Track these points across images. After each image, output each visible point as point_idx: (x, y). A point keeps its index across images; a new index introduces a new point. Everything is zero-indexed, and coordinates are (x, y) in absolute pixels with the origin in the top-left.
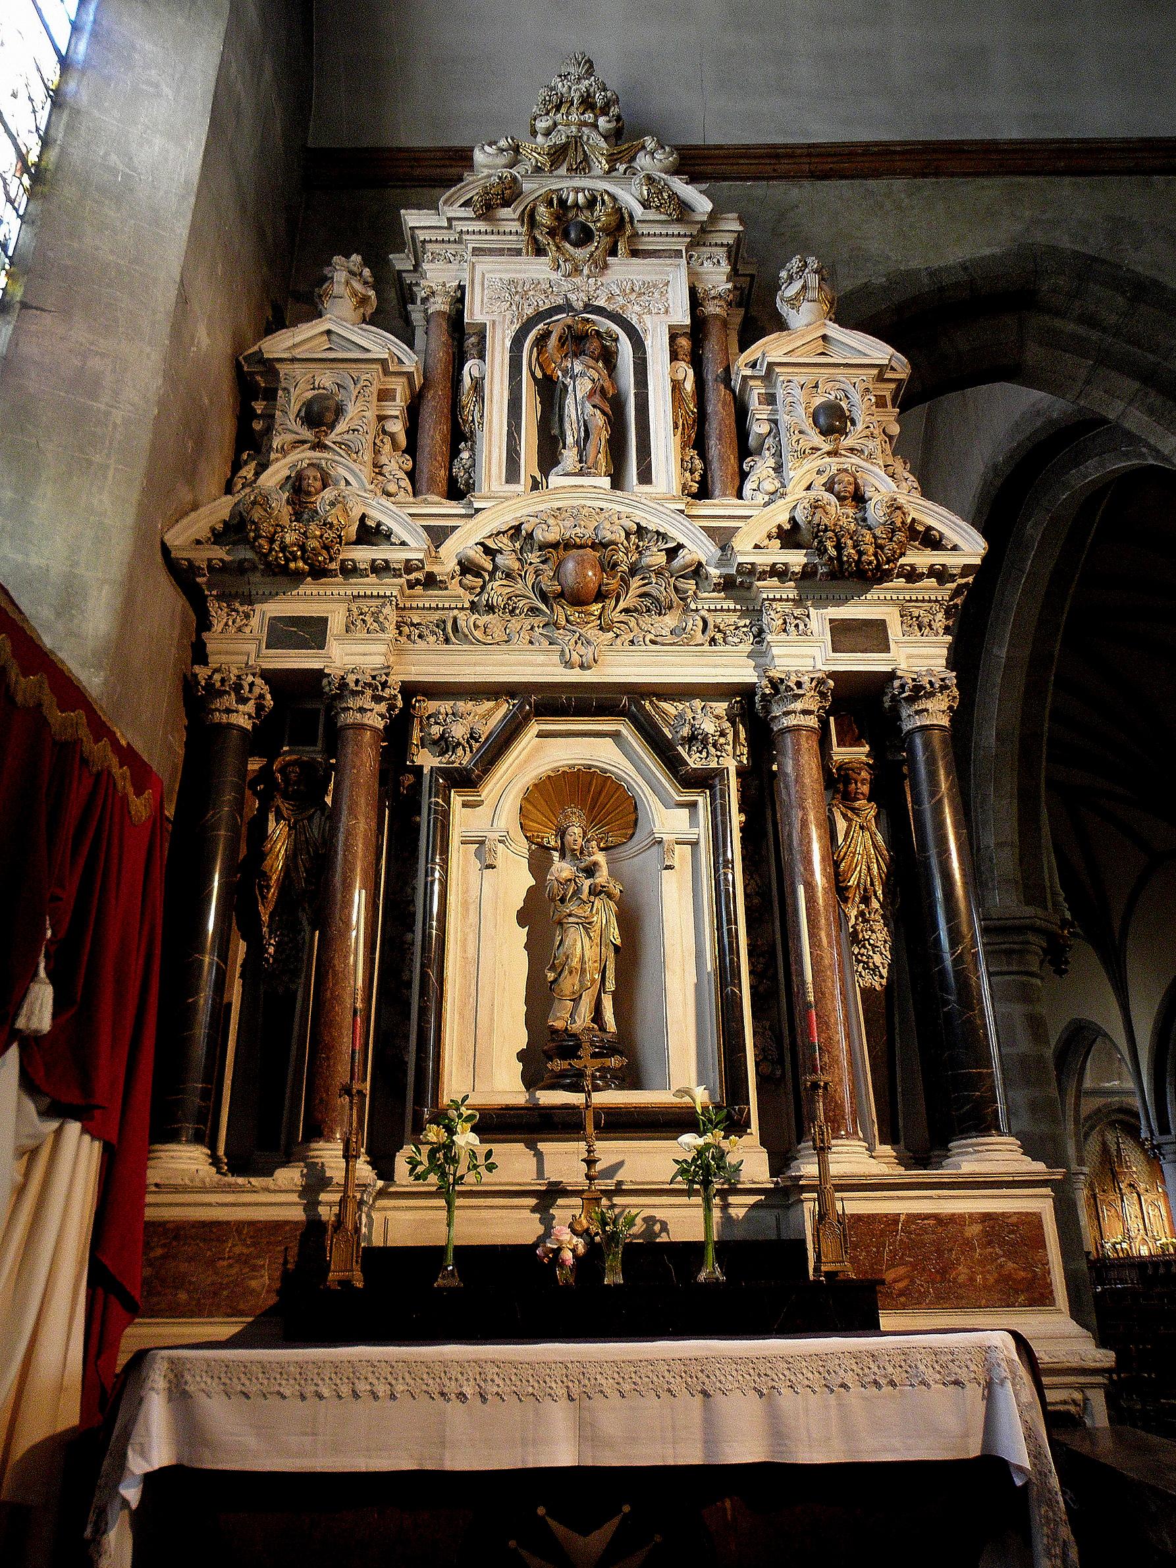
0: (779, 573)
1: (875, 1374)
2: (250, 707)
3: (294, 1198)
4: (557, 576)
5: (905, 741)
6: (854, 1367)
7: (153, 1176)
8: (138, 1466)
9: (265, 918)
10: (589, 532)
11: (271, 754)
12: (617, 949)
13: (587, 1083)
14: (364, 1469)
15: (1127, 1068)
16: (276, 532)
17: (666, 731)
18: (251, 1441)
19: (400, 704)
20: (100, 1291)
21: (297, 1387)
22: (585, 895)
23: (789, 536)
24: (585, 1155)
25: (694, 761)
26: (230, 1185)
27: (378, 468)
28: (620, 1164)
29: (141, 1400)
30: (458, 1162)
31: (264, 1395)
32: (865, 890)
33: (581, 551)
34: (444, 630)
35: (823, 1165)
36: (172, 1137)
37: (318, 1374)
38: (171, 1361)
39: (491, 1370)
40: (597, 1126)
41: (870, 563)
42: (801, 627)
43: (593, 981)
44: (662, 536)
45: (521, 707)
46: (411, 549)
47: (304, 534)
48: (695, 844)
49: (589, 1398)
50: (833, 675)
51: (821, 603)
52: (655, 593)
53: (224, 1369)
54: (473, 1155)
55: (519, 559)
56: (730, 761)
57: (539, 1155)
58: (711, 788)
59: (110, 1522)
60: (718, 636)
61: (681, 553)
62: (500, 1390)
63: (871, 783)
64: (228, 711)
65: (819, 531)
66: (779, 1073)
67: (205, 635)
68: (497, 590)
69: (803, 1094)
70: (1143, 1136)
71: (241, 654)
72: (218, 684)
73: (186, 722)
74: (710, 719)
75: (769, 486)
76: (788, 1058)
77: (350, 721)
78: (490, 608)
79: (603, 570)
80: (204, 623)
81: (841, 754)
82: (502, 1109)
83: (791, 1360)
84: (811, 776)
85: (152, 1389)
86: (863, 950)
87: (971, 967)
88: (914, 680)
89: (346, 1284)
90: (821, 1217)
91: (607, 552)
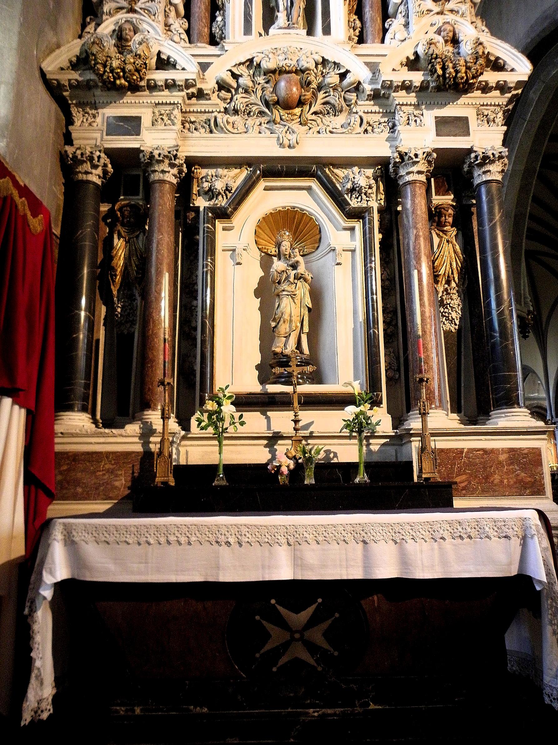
0: (406, 87)
1: (460, 532)
2: (99, 171)
3: (136, 440)
4: (275, 91)
5: (474, 192)
6: (449, 528)
7: (58, 428)
8: (49, 579)
9: (115, 293)
10: (294, 63)
11: (113, 200)
12: (309, 310)
13: (294, 380)
14: (174, 581)
15: (542, 388)
16: (107, 61)
17: (338, 185)
18: (112, 567)
19: (185, 170)
20: (33, 488)
21: (136, 539)
22: (292, 279)
23: (413, 64)
24: (293, 418)
25: (354, 203)
26: (101, 433)
27: (167, 26)
28: (312, 422)
29: (49, 545)
30: (224, 420)
31: (118, 543)
32: (448, 277)
33: (289, 75)
34: (209, 125)
35: (424, 422)
36: (70, 408)
37: (147, 532)
38: (65, 525)
39: (244, 530)
40: (299, 403)
41: (462, 78)
42: (418, 121)
43: (297, 327)
44: (337, 65)
45: (254, 172)
46: (188, 73)
47: (124, 61)
48: (353, 251)
49: (300, 544)
50: (435, 150)
51: (430, 106)
52: (332, 101)
53: (95, 529)
54: (233, 417)
55: (253, 81)
56: (375, 202)
57: (268, 418)
58: (363, 218)
59: (37, 607)
60: (369, 129)
61: (348, 75)
62: (249, 541)
63: (454, 217)
64: (87, 173)
65: (432, 59)
66: (397, 376)
67: (70, 128)
68: (240, 100)
69: (411, 385)
70: (548, 418)
71: (92, 139)
72: (79, 157)
73: (63, 181)
74: (363, 178)
75: (399, 36)
76: (402, 368)
77: (156, 178)
78: (236, 112)
79: (302, 87)
80: (70, 121)
81: (437, 200)
82: (247, 394)
83: (413, 525)
84: (421, 210)
85: (55, 539)
86: (446, 310)
87: (508, 317)
88: (483, 153)
89: (165, 483)
90: (423, 450)
91: (305, 75)
